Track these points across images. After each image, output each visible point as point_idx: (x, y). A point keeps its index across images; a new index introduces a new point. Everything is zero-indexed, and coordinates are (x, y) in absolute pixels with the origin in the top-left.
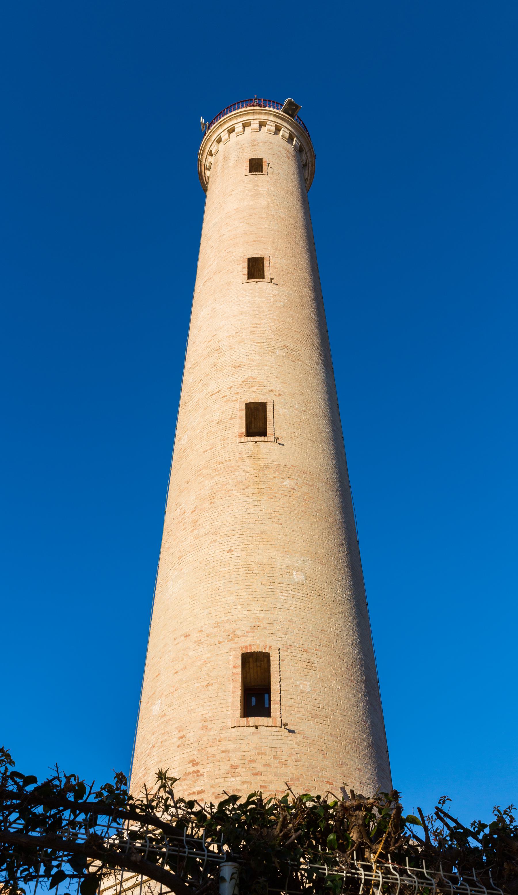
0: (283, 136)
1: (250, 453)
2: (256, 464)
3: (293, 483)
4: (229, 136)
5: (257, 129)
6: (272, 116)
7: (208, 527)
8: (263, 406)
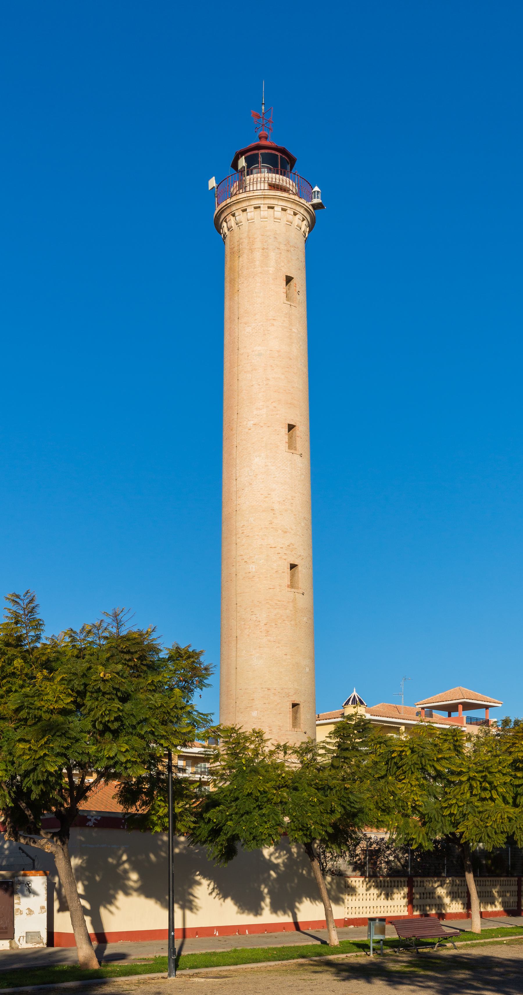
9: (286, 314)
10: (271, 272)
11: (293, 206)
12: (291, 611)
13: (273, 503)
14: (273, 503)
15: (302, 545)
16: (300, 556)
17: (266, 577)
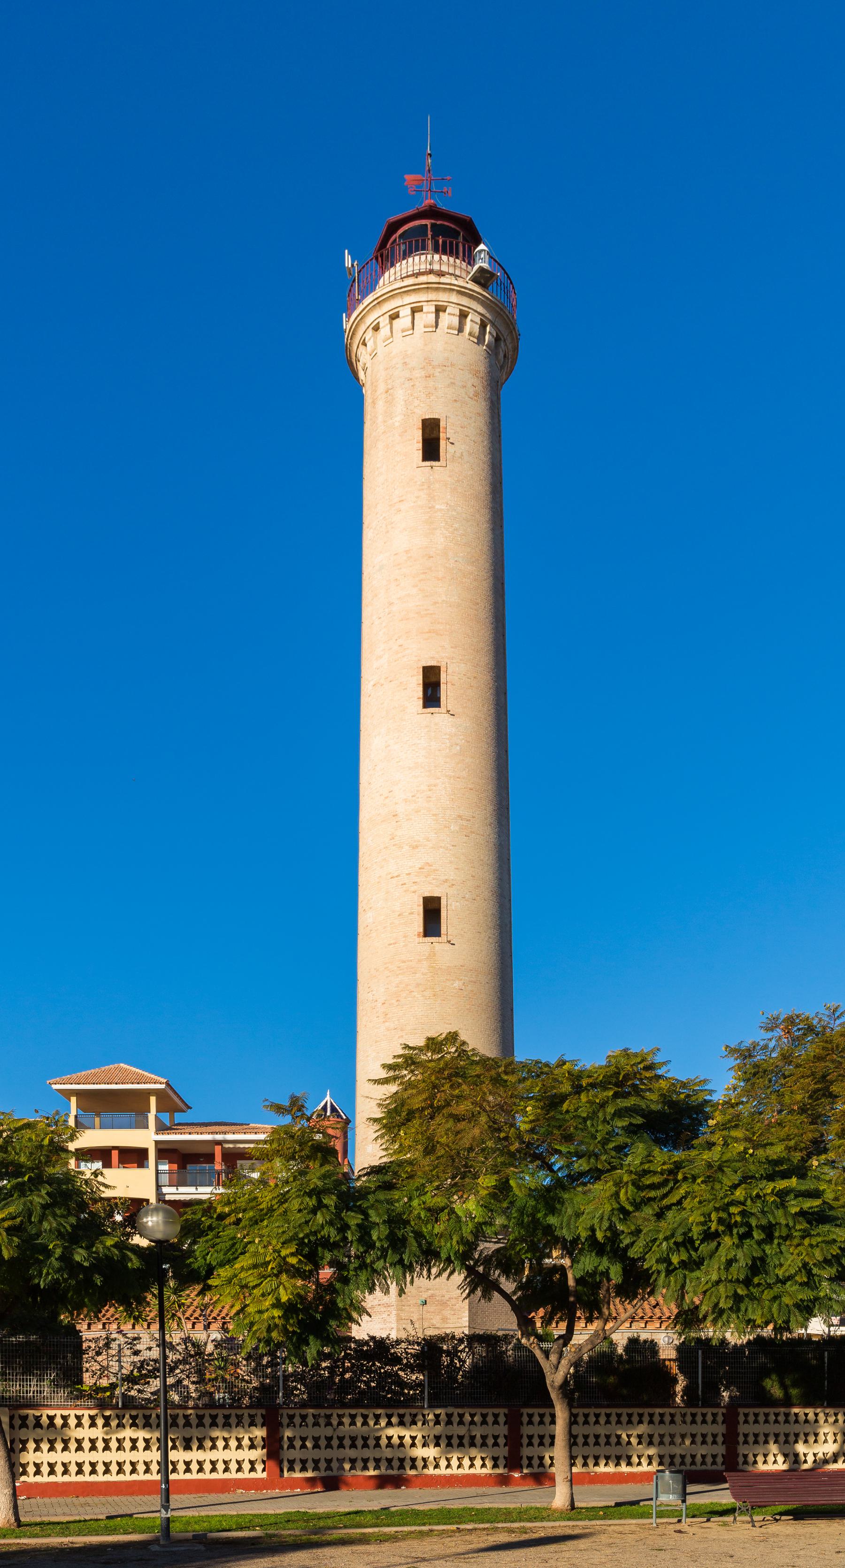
0: (470, 334)
1: (427, 954)
2: (432, 967)
3: (461, 983)
4: (391, 324)
5: (432, 327)
6: (455, 293)
7: (396, 1022)
8: (438, 899)
9: (423, 484)
10: (397, 424)
11: (432, 296)
12: (423, 974)
13: (396, 803)
14: (396, 803)
15: (451, 862)
16: (446, 881)
17: (385, 928)
